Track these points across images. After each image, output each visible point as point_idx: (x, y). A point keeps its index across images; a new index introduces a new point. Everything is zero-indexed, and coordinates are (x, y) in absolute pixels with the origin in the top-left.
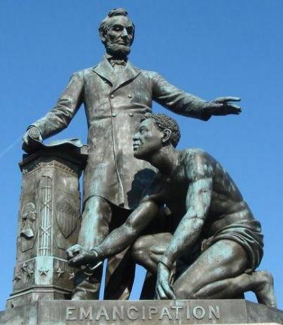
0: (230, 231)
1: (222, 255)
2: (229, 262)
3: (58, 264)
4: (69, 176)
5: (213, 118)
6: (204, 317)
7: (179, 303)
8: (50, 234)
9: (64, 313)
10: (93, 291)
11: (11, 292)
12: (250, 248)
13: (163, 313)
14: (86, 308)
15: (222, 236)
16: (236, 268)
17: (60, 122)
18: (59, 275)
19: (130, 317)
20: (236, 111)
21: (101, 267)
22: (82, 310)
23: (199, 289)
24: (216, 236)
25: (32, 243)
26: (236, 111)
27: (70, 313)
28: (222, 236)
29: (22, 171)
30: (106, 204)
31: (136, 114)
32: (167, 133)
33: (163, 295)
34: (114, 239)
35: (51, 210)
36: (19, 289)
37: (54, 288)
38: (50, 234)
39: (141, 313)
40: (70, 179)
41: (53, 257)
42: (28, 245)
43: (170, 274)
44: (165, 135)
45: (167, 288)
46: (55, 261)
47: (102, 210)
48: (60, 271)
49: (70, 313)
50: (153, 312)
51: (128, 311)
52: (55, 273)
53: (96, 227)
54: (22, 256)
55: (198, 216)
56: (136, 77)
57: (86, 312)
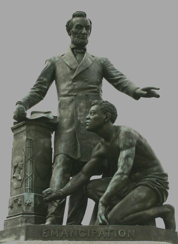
0: (146, 181)
1: (140, 196)
2: (144, 200)
3: (37, 198)
4: (44, 138)
5: (142, 98)
6: (124, 237)
7: (111, 227)
8: (33, 178)
9: (42, 233)
10: (59, 217)
11: (7, 216)
12: (160, 193)
13: (100, 233)
14: (54, 230)
15: (141, 183)
16: (149, 204)
17: (38, 97)
18: (38, 205)
19: (81, 236)
20: (158, 96)
21: (65, 179)
22: (52, 231)
23: (124, 218)
24: (137, 183)
25: (21, 184)
26: (158, 96)
27: (45, 233)
28: (141, 183)
29: (13, 132)
30: (68, 159)
31: (90, 94)
32: (108, 115)
33: (101, 222)
34: (73, 181)
35: (33, 162)
36: (14, 213)
37: (34, 214)
38: (33, 178)
39: (87, 233)
40: (45, 139)
41: (34, 194)
42: (18, 184)
43: (106, 209)
44: (107, 117)
45: (103, 218)
46: (35, 196)
47: (65, 163)
48: (38, 203)
49: (45, 233)
50: (94, 233)
51: (80, 232)
52: (35, 204)
53: (60, 176)
54: (14, 192)
55: (125, 173)
56: (91, 64)
57: (55, 233)
